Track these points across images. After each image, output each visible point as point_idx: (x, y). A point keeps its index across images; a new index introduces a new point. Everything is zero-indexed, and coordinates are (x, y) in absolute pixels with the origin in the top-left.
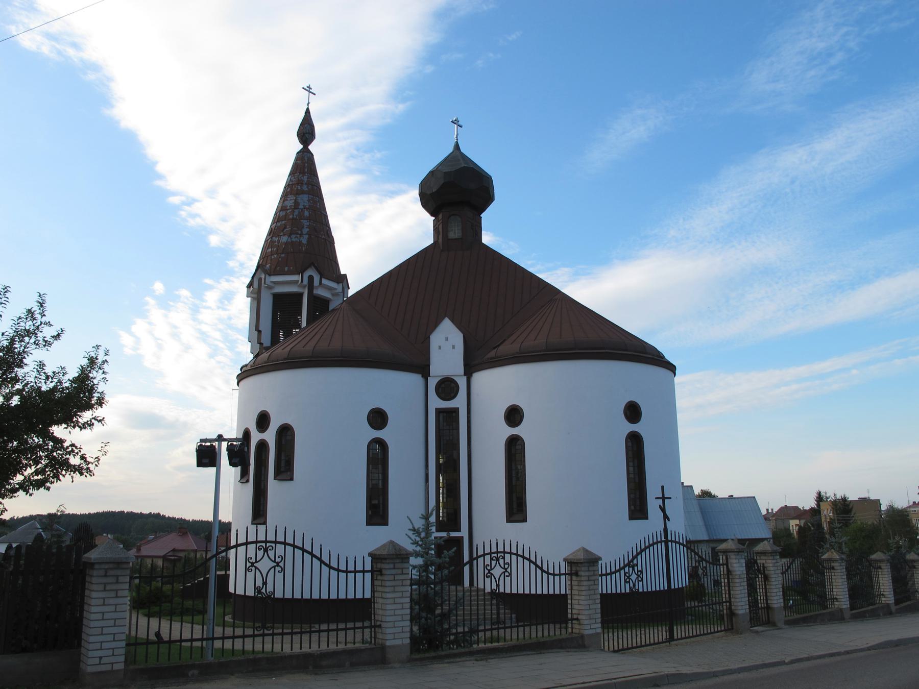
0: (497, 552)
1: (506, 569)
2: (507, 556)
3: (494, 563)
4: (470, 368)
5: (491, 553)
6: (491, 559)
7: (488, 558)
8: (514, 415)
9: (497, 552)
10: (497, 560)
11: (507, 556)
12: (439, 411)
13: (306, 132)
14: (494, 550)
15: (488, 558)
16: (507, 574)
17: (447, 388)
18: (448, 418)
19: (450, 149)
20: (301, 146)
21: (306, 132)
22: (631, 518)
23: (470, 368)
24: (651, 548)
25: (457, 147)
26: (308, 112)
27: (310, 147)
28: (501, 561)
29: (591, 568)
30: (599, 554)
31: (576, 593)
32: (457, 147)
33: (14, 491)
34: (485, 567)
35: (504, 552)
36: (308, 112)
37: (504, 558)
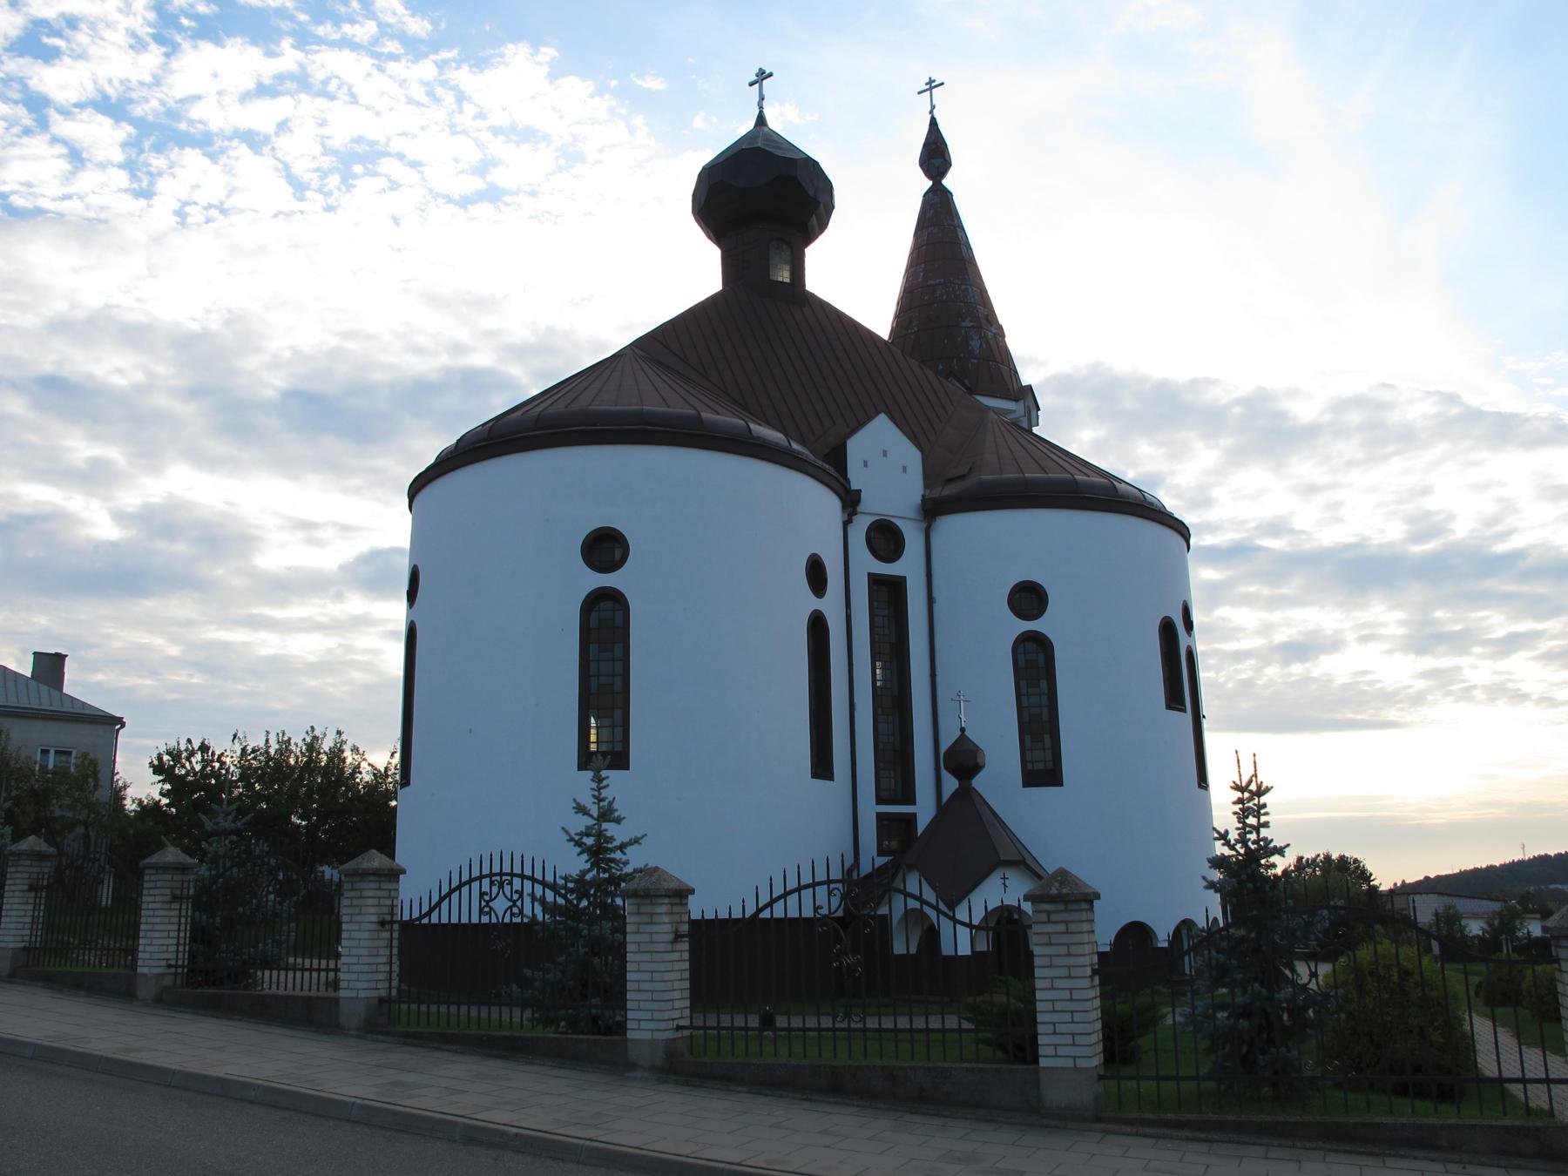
0: (501, 874)
1: (515, 902)
2: (517, 882)
3: (495, 889)
4: (932, 510)
5: (491, 875)
6: (492, 883)
7: (486, 882)
8: (1028, 599)
9: (501, 874)
10: (501, 886)
11: (517, 882)
12: (875, 581)
13: (935, 156)
14: (496, 869)
15: (486, 882)
16: (515, 910)
17: (886, 539)
18: (888, 593)
19: (749, 125)
20: (945, 182)
21: (935, 156)
22: (1061, 784)
23: (932, 510)
24: (465, 889)
25: (761, 120)
26: (933, 123)
27: (945, 182)
28: (507, 889)
29: (644, 909)
30: (688, 880)
31: (381, 968)
32: (761, 120)
33: (1449, 693)
34: (482, 894)
35: (512, 874)
36: (933, 123)
37: (511, 883)
